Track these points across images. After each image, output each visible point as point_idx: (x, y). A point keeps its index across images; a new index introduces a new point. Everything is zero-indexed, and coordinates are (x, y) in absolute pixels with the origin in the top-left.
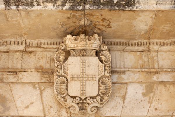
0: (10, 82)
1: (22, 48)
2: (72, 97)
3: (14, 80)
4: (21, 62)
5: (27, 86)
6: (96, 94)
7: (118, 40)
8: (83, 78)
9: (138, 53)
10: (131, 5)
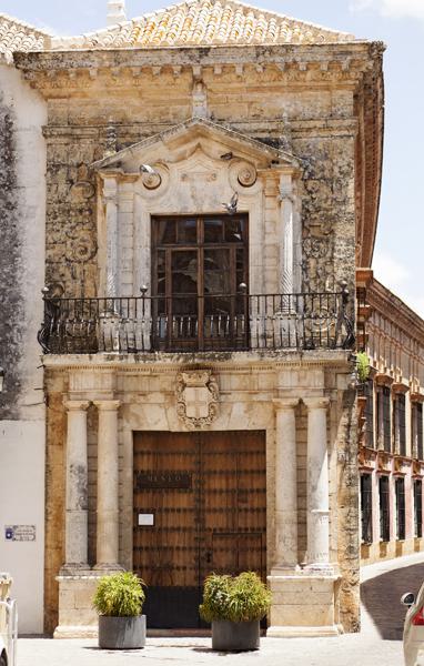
1: (149, 373)
8: (197, 403)
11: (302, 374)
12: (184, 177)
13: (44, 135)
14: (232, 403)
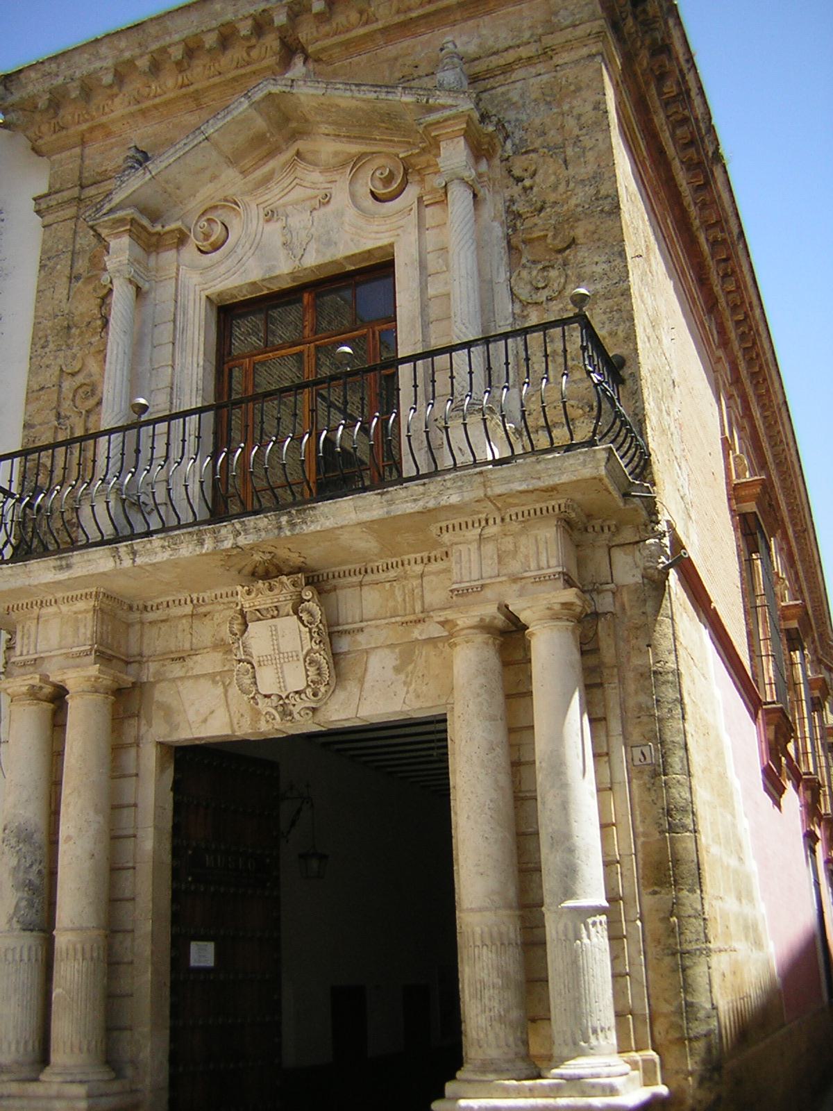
0: (177, 678)
1: (188, 609)
2: (266, 696)
3: (181, 674)
4: (189, 636)
5: (202, 680)
6: (305, 685)
7: (346, 568)
8: (279, 658)
9: (388, 585)
11: (508, 543)
12: (270, 216)
13: (38, 212)
14: (367, 652)
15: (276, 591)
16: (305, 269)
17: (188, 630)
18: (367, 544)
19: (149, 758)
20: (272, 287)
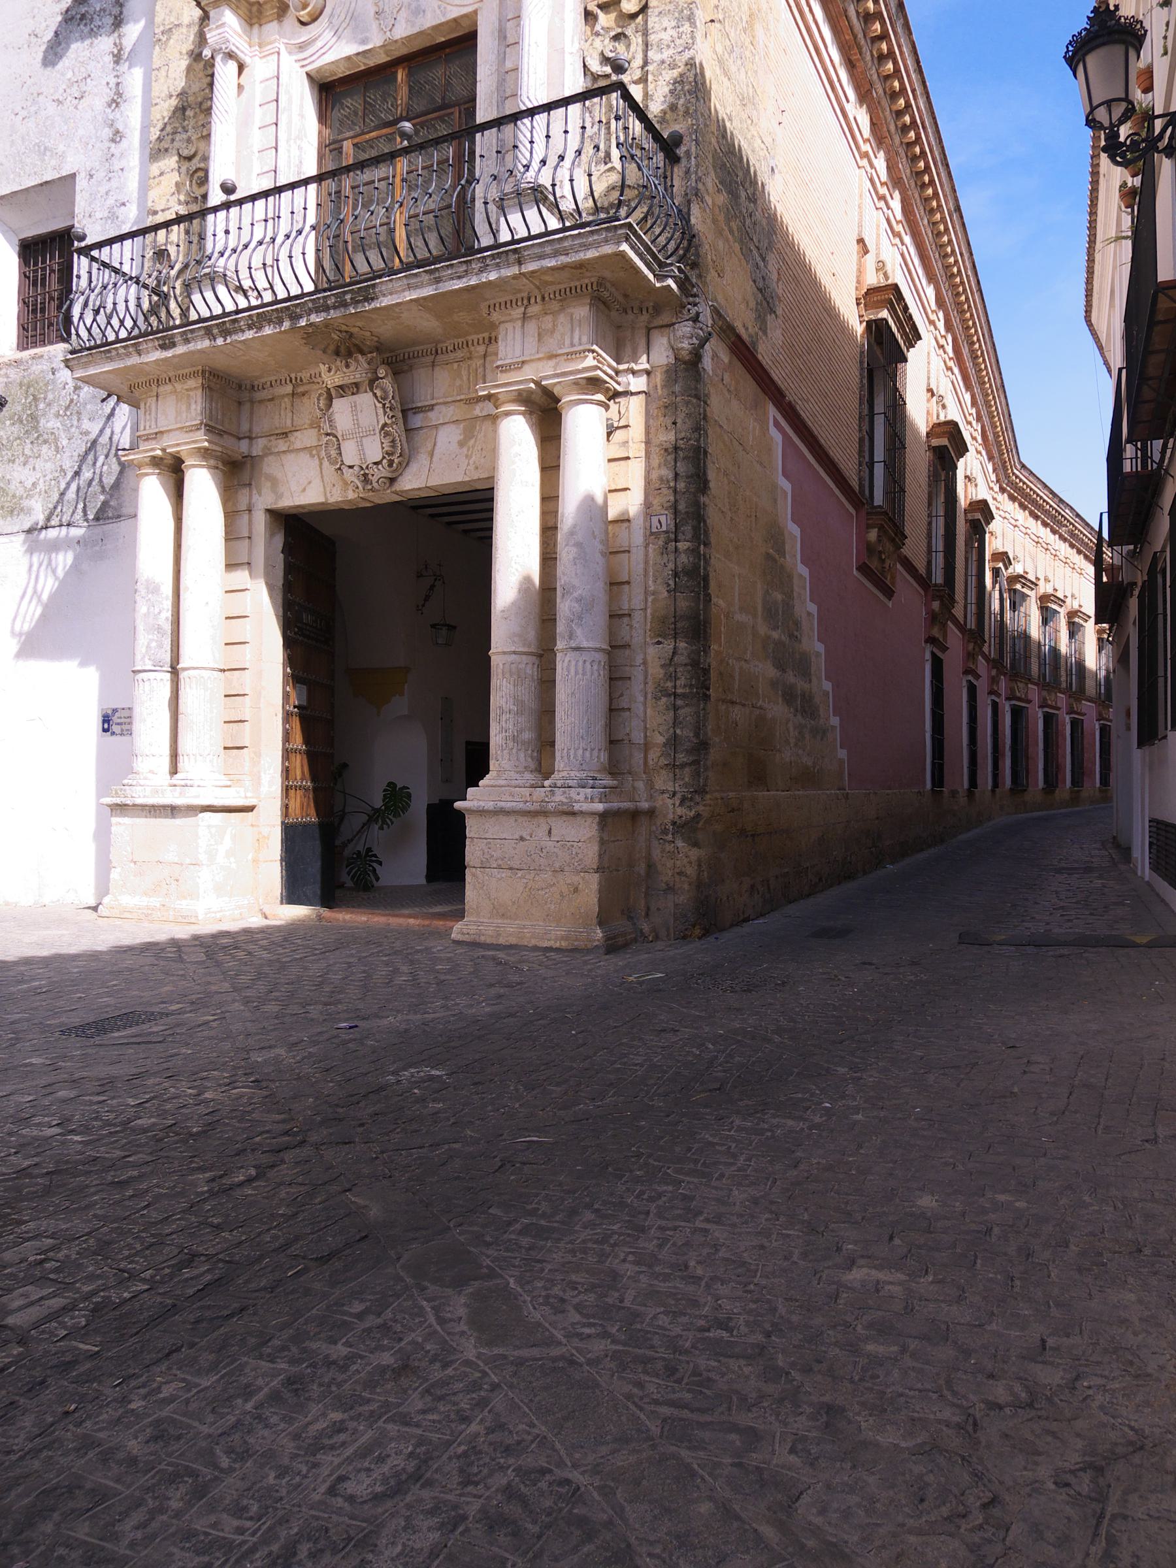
3: (285, 449)
5: (302, 454)
9: (455, 365)
10: (372, 299)
15: (352, 368)
16: (396, 41)
17: (289, 407)
18: (428, 324)
19: (260, 521)
20: (367, 61)
